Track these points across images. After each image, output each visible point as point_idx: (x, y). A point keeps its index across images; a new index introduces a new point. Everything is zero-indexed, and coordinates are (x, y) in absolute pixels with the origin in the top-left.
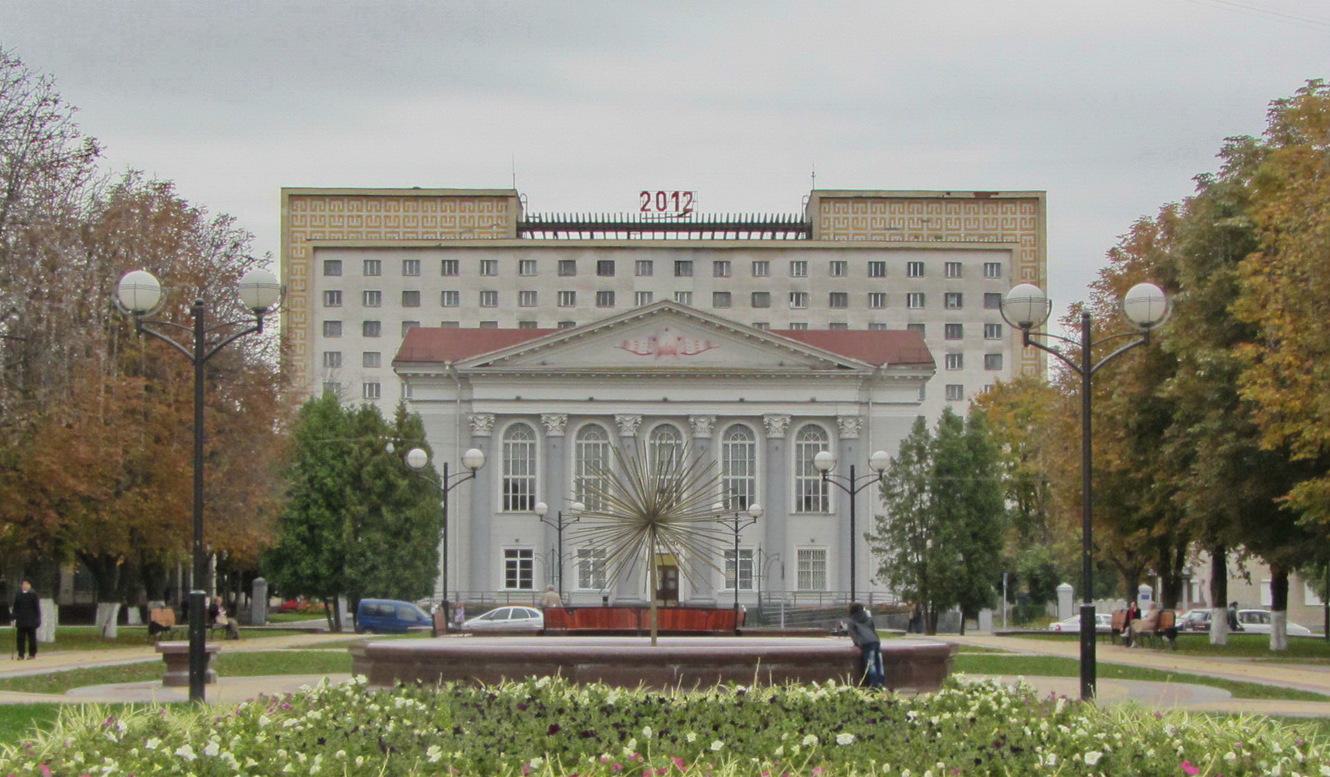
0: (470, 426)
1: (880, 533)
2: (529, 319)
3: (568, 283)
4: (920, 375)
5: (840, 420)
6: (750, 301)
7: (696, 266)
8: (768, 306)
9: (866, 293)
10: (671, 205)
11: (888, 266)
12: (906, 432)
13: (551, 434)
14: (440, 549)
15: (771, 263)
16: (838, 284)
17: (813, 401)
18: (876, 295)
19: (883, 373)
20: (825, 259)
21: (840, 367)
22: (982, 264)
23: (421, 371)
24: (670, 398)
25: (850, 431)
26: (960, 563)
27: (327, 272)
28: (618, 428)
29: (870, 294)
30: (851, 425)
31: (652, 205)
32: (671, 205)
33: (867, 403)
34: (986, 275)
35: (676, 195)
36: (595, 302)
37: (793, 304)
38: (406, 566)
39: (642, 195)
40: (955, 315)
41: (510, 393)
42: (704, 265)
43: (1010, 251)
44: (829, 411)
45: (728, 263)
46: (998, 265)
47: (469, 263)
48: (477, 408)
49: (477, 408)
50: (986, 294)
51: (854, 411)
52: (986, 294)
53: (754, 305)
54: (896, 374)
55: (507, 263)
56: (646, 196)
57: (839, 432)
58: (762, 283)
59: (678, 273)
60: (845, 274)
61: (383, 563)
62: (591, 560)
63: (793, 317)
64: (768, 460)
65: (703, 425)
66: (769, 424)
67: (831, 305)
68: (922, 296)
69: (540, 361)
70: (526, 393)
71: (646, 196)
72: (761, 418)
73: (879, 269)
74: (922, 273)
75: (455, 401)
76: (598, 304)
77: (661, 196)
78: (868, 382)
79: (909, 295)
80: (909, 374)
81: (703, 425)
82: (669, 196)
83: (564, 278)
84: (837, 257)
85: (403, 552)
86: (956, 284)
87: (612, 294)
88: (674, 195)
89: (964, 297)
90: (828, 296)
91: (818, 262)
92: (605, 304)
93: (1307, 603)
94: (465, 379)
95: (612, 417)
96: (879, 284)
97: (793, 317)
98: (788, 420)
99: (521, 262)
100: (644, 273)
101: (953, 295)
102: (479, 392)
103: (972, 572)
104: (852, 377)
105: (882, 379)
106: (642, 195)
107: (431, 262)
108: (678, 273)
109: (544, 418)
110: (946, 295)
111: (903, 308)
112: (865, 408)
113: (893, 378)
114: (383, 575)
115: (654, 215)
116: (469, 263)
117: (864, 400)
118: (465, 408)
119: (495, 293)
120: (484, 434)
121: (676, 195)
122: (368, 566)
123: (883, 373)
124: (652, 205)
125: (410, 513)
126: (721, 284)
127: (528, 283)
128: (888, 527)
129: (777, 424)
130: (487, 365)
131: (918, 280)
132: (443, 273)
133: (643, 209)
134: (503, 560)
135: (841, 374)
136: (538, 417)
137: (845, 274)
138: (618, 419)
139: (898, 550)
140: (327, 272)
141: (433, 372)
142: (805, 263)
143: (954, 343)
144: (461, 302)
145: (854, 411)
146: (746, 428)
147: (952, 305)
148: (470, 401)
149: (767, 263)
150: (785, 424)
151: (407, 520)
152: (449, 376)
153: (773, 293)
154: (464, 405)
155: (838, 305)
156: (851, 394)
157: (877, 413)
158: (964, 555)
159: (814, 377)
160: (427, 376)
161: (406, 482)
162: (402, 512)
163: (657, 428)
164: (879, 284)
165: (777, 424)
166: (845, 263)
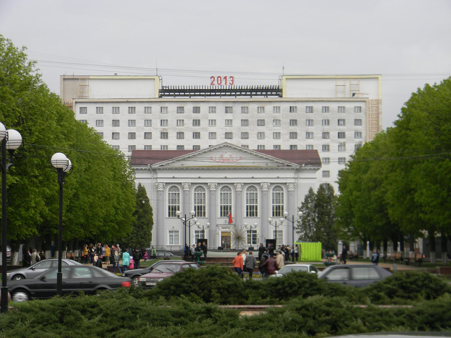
0: (157, 187)
1: (298, 227)
2: (165, 132)
3: (181, 116)
4: (316, 168)
5: (288, 184)
6: (256, 123)
7: (234, 109)
8: (264, 125)
9: (305, 120)
10: (223, 83)
11: (314, 108)
12: (307, 193)
13: (185, 190)
14: (153, 232)
15: (266, 108)
16: (293, 116)
17: (278, 178)
18: (309, 120)
19: (303, 168)
20: (288, 105)
21: (288, 165)
22: (353, 107)
23: (139, 168)
24: (227, 177)
25: (291, 188)
26: (325, 236)
27: (81, 112)
28: (209, 188)
29: (307, 120)
30: (291, 186)
31: (215, 82)
32: (223, 83)
33: (297, 178)
34: (355, 111)
35: (225, 78)
36: (192, 124)
37: (274, 124)
38: (142, 238)
39: (211, 78)
40: (342, 128)
41: (170, 175)
42: (237, 108)
43: (365, 101)
44: (284, 181)
45: (247, 107)
46: (360, 107)
47: (140, 108)
48: (159, 181)
49: (159, 181)
50: (355, 120)
51: (293, 181)
52: (355, 120)
53: (258, 125)
54: (308, 168)
55: (156, 108)
56: (213, 79)
57: (288, 188)
58: (262, 116)
59: (226, 112)
60: (296, 112)
61: (134, 237)
62: (200, 234)
63: (274, 130)
64: (262, 197)
65: (239, 186)
66: (263, 186)
67: (290, 125)
68: (328, 120)
69: (181, 164)
70: (176, 175)
71: (213, 79)
72: (260, 183)
73: (311, 110)
74: (328, 111)
75: (151, 178)
76: (193, 125)
77: (219, 79)
78: (298, 170)
79: (323, 120)
80: (312, 168)
81: (239, 186)
82: (222, 79)
83: (179, 114)
84: (292, 105)
85: (141, 233)
86: (342, 116)
87: (199, 120)
88: (224, 78)
89: (346, 121)
90: (289, 121)
91: (285, 107)
92: (196, 125)
93: (204, 257)
94: (155, 170)
95: (207, 183)
96: (311, 116)
97: (274, 130)
98: (269, 184)
99: (161, 108)
100: (212, 112)
101: (341, 120)
102: (160, 175)
103: (329, 239)
104: (292, 169)
105: (303, 169)
106: (211, 78)
107: (124, 108)
108: (226, 112)
109: (183, 184)
110: (339, 120)
111: (320, 126)
112: (297, 180)
113: (306, 169)
114: (135, 241)
115: (216, 86)
116: (140, 108)
117: (296, 177)
118: (154, 181)
119: (151, 120)
120: (162, 190)
121: (225, 78)
122: (130, 238)
123: (303, 168)
124: (215, 82)
125: (143, 220)
126: (244, 116)
127: (164, 116)
128: (301, 224)
129: (265, 186)
130: (163, 165)
131: (327, 114)
132: (129, 113)
133: (211, 84)
134: (168, 234)
135: (288, 168)
136: (181, 183)
137: (296, 112)
138: (209, 184)
139: (304, 232)
140: (81, 112)
141: (143, 168)
142: (279, 107)
143: (342, 140)
144: (137, 124)
145: (293, 181)
146: (254, 187)
147: (341, 124)
148: (157, 178)
149: (263, 107)
150: (268, 186)
151: (142, 222)
152: (149, 169)
153: (266, 120)
154: (154, 180)
155: (293, 125)
156: (291, 175)
157: (301, 181)
158: (327, 233)
159: (278, 169)
160: (141, 169)
161: (142, 210)
162: (140, 220)
163: (223, 187)
164: (311, 116)
165: (265, 186)
166: (296, 107)
